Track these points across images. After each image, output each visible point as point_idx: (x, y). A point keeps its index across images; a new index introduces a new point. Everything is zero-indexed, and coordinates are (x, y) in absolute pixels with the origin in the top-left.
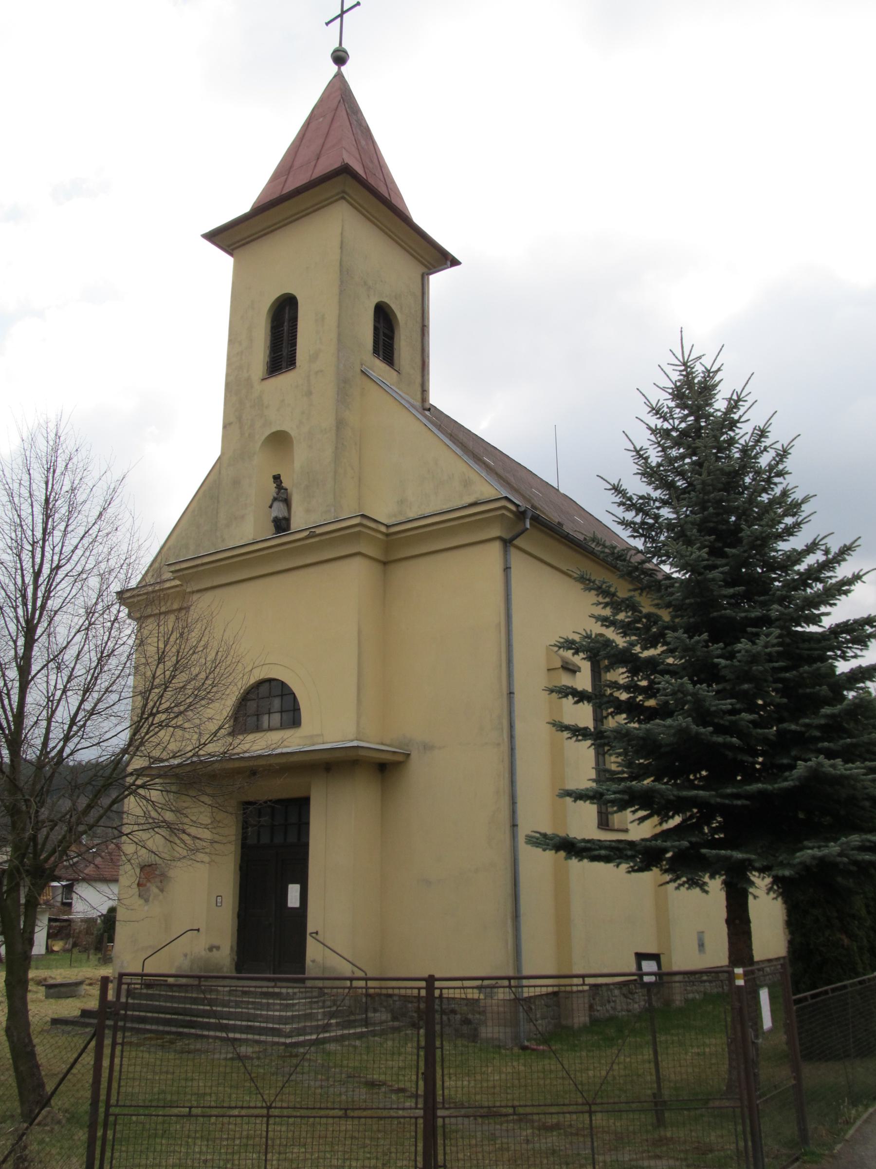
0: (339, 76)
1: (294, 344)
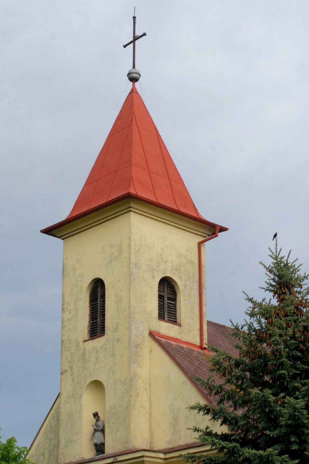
0: (133, 92)
1: (104, 316)
